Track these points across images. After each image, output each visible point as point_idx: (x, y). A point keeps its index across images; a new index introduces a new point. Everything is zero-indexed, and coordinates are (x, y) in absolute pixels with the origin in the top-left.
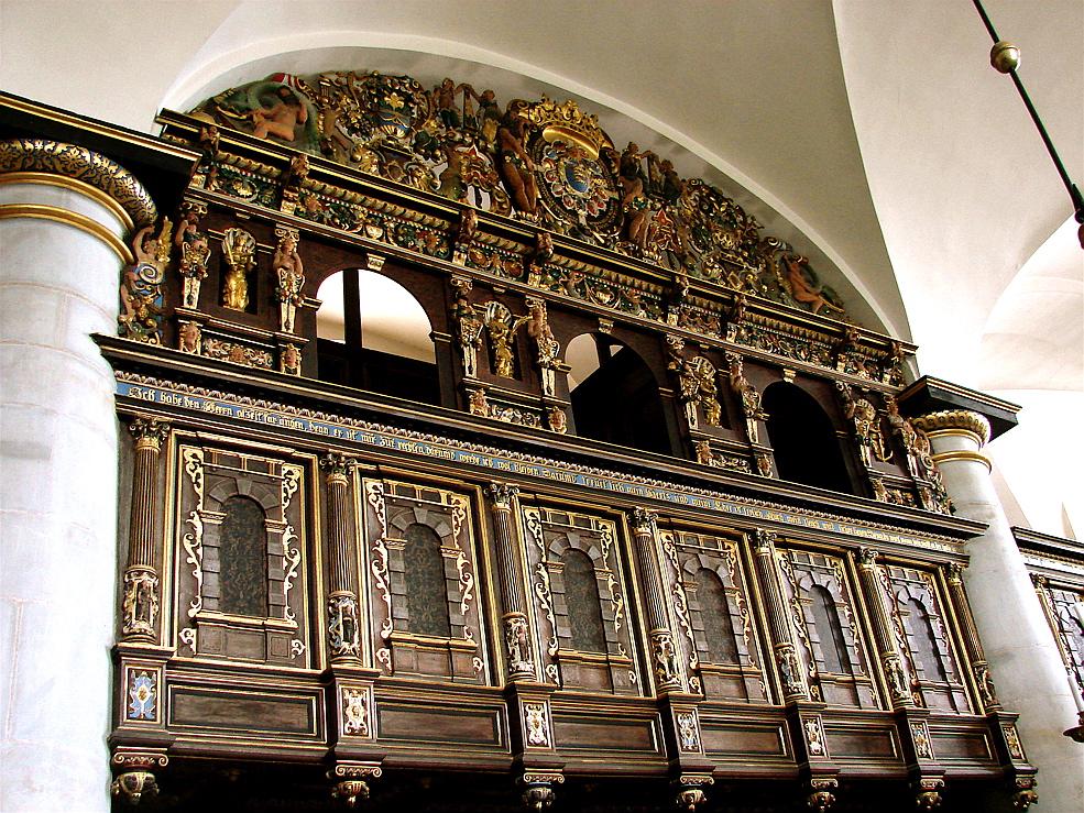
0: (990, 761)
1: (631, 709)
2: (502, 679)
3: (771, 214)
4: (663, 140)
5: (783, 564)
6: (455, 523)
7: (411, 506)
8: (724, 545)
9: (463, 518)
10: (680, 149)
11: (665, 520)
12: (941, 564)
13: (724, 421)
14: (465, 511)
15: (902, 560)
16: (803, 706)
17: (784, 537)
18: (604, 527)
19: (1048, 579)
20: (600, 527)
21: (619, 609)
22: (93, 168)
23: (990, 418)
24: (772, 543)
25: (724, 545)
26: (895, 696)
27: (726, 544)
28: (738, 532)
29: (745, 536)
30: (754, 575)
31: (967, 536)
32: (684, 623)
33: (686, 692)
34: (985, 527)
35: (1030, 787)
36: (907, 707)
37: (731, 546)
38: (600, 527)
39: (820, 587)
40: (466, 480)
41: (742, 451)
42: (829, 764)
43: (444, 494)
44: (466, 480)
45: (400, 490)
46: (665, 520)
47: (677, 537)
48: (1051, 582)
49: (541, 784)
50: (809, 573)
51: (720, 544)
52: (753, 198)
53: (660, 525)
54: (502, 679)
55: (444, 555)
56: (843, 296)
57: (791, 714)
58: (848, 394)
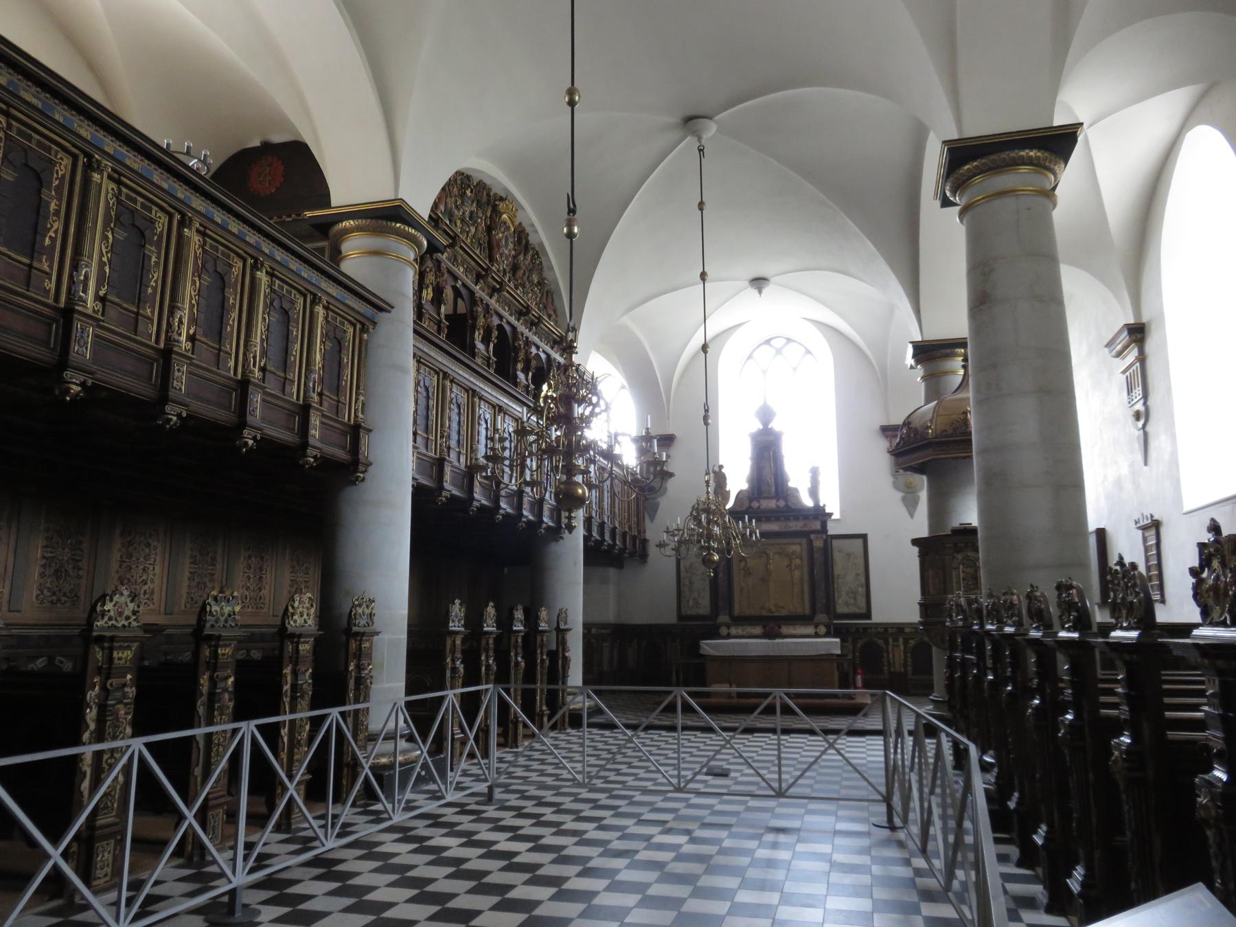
0: (152, 385)
1: (143, 349)
2: (63, 298)
3: (551, 268)
4: (533, 225)
5: (197, 246)
6: (55, 176)
7: (216, 259)
8: (156, 214)
9: (63, 172)
10: (536, 231)
11: (116, 176)
12: (311, 292)
13: (432, 302)
14: (66, 168)
15: (295, 284)
16: (80, 313)
17: (205, 228)
18: (61, 159)
19: (420, 357)
20: (59, 157)
21: (155, 278)
22: (414, 236)
23: (429, 242)
24: (105, 174)
25: (156, 214)
26: (356, 416)
27: (158, 215)
28: (76, 151)
29: (309, 296)
30: (307, 322)
31: (381, 309)
32: (105, 259)
33: (90, 312)
34: (392, 307)
35: (363, 472)
36: (252, 379)
37: (163, 218)
38: (59, 157)
39: (337, 339)
40: (245, 252)
41: (436, 319)
42: (318, 444)
43: (155, 208)
44: (245, 252)
45: (211, 247)
46: (116, 176)
47: (205, 242)
48: (422, 360)
49: (173, 413)
50: (281, 298)
51: (154, 213)
52: (549, 260)
53: (110, 177)
54: (63, 298)
55: (43, 196)
56: (558, 312)
57: (244, 385)
58: (493, 312)
